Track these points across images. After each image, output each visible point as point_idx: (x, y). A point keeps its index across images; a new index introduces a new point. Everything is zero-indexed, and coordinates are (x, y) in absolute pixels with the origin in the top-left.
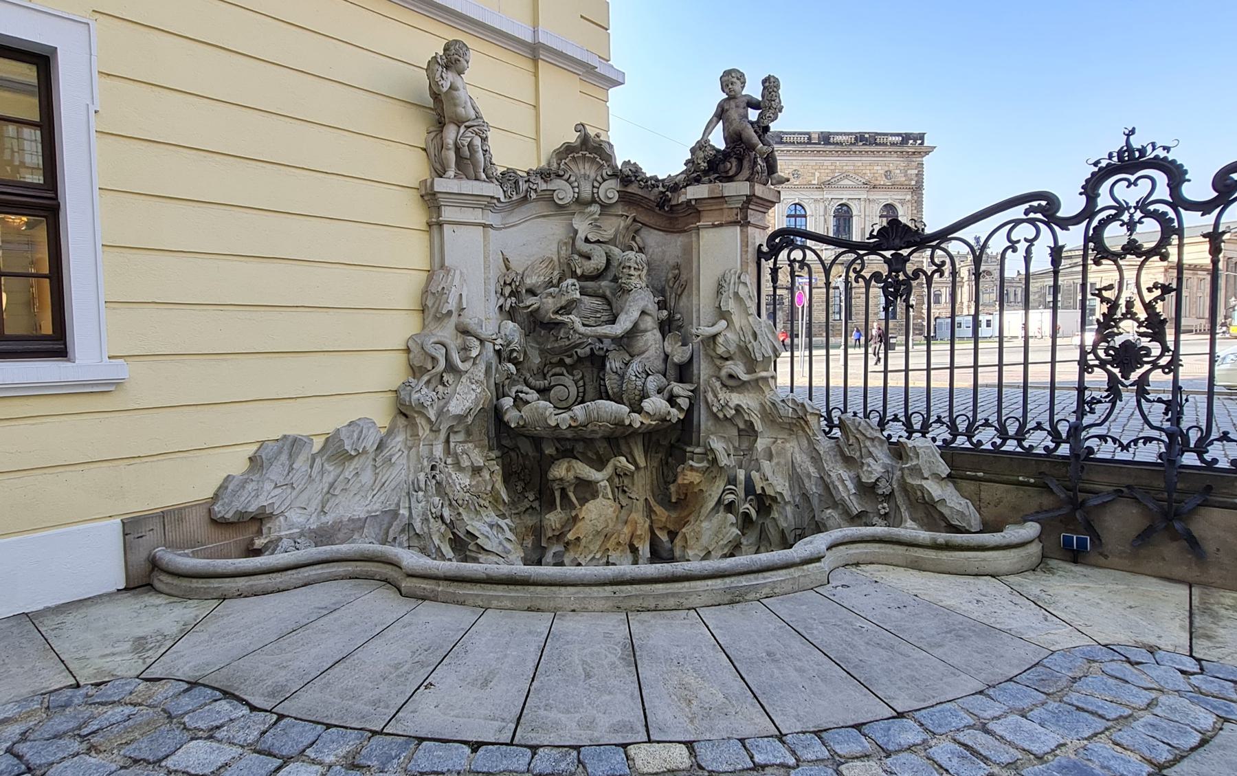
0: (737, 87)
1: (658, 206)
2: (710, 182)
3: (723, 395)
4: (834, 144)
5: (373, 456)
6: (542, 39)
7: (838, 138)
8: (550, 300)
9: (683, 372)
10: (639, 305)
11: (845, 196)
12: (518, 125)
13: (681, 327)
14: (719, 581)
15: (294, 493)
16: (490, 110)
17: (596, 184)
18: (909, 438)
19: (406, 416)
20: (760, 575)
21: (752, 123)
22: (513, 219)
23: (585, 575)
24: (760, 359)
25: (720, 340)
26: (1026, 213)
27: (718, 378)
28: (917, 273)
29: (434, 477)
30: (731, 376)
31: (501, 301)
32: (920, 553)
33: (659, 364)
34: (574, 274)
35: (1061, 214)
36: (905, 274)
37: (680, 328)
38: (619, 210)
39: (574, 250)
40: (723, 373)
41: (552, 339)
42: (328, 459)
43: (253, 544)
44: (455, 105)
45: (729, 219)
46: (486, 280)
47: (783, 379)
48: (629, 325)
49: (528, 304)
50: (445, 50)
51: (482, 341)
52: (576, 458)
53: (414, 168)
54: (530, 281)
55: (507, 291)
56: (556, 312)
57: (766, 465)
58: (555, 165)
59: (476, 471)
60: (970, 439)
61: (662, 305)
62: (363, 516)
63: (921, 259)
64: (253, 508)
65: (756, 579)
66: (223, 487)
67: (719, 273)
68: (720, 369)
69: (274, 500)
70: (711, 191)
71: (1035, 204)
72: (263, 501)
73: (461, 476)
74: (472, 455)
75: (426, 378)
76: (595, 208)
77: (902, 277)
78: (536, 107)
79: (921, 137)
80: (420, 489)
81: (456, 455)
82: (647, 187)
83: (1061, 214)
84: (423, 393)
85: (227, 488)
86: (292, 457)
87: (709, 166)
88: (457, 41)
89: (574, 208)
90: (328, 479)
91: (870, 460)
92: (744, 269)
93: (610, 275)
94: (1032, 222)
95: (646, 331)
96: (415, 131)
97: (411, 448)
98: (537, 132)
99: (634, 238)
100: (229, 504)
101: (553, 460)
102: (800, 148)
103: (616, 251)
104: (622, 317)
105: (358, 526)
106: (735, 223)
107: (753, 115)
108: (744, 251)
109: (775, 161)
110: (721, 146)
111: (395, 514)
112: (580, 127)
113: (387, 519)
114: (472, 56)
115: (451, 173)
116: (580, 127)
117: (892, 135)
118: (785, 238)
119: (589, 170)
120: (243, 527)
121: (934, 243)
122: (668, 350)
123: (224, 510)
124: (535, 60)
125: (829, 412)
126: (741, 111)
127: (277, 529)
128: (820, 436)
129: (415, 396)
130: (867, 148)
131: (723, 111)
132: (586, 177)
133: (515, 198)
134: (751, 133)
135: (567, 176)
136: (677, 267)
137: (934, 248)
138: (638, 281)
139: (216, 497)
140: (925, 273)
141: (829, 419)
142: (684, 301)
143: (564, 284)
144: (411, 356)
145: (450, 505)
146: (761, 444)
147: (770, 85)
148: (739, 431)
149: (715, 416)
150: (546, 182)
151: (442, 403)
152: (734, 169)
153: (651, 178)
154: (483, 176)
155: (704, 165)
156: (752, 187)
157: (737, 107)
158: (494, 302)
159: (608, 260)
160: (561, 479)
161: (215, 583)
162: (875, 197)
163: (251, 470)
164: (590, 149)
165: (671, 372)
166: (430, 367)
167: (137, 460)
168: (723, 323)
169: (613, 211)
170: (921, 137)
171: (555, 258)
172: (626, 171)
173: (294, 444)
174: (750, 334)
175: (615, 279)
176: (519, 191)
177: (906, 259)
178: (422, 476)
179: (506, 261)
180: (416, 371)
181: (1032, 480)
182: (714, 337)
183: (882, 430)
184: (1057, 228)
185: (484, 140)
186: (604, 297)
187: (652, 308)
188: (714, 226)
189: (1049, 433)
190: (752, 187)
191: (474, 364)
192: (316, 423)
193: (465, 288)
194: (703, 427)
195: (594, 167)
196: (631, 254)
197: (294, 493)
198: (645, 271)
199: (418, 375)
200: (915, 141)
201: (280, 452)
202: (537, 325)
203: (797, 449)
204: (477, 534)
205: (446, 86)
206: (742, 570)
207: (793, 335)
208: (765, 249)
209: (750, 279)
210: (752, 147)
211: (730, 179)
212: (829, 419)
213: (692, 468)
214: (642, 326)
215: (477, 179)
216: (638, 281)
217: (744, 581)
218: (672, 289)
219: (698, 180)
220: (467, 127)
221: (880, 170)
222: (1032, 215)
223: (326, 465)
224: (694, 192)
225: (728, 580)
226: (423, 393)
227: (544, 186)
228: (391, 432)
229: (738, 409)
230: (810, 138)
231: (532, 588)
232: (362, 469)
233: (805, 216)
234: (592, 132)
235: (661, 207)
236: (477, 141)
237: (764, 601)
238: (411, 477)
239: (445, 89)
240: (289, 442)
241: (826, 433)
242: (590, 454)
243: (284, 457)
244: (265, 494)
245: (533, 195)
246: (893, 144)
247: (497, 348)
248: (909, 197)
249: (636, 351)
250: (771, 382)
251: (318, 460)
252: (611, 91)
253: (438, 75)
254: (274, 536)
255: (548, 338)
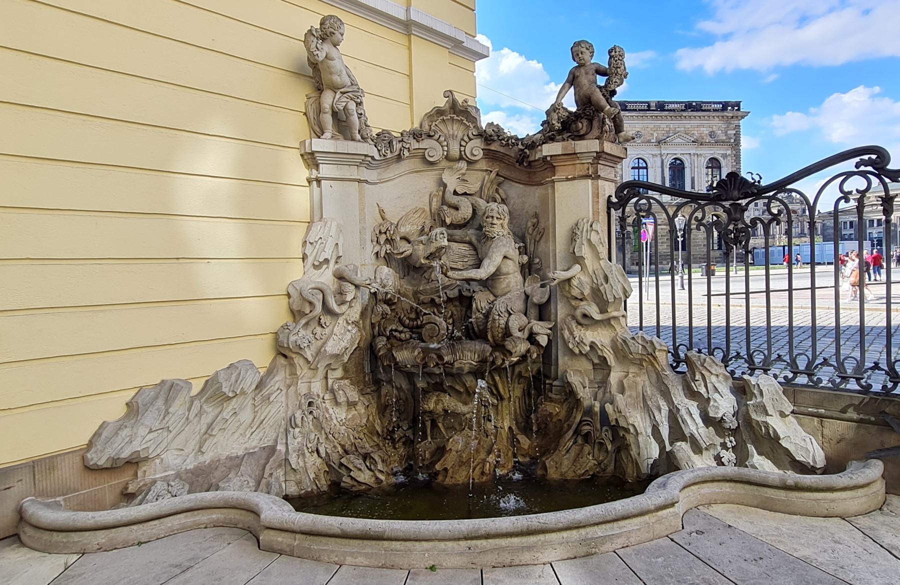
0: (587, 56)
1: (517, 162)
2: (564, 140)
3: (579, 332)
4: (668, 110)
5: (253, 395)
6: (414, 17)
7: (671, 106)
8: (421, 247)
9: (543, 312)
10: (503, 255)
11: (678, 152)
12: (391, 89)
13: (539, 270)
14: (574, 532)
15: (171, 436)
16: (365, 79)
17: (463, 143)
18: (751, 375)
19: (285, 356)
20: (615, 524)
21: (600, 88)
22: (387, 175)
23: (439, 531)
24: (611, 300)
25: (575, 282)
26: (857, 166)
27: (574, 317)
28: (754, 221)
29: (311, 413)
30: (585, 316)
31: (377, 248)
32: (770, 493)
33: (519, 305)
34: (443, 223)
35: (891, 167)
36: (744, 223)
37: (538, 271)
38: (483, 165)
39: (444, 202)
40: (578, 313)
41: (424, 281)
42: (206, 401)
43: (127, 488)
44: (331, 73)
45: (581, 173)
46: (362, 231)
47: (633, 320)
48: (492, 270)
49: (401, 251)
50: (321, 24)
51: (357, 287)
52: (445, 392)
53: (295, 127)
54: (404, 230)
55: (383, 238)
56: (427, 258)
57: (619, 398)
58: (427, 127)
59: (351, 405)
60: (810, 375)
61: (523, 251)
62: (240, 453)
63: (754, 211)
64: (125, 454)
65: (612, 529)
66: (97, 434)
67: (572, 222)
68: (575, 308)
69: (148, 444)
70: (564, 148)
71: (866, 157)
72: (136, 446)
73: (337, 410)
74: (348, 391)
75: (303, 321)
76: (463, 165)
77: (740, 226)
78: (410, 76)
79: (738, 104)
80: (296, 426)
81: (332, 391)
82: (508, 145)
83: (891, 167)
84: (301, 335)
85: (100, 435)
86: (168, 401)
87: (563, 126)
88: (331, 16)
89: (444, 164)
90: (206, 420)
91: (716, 396)
92: (596, 219)
93: (476, 223)
94: (863, 174)
95: (508, 274)
96: (298, 96)
97: (289, 386)
98: (411, 98)
99: (497, 191)
100: (101, 452)
101: (425, 392)
102: (642, 114)
103: (482, 203)
104: (486, 262)
105: (235, 463)
106: (588, 176)
107: (601, 81)
108: (596, 202)
109: (621, 121)
110: (573, 109)
111: (272, 450)
112: (449, 94)
113: (264, 455)
114: (347, 29)
115: (328, 134)
116: (449, 94)
117: (715, 103)
118: (630, 190)
119: (457, 130)
120: (115, 474)
121: (771, 194)
122: (529, 290)
123: (99, 458)
124: (409, 35)
125: (676, 349)
126: (591, 77)
127: (150, 472)
128: (668, 372)
129: (293, 338)
130: (695, 114)
131: (574, 77)
132: (454, 137)
133: (389, 155)
134: (599, 96)
135: (437, 136)
136: (536, 216)
137: (770, 199)
138: (500, 229)
139: (90, 444)
140: (762, 222)
141: (676, 355)
142: (542, 246)
143: (433, 233)
144: (291, 300)
145: (327, 438)
146: (614, 377)
147: (615, 55)
148: (594, 364)
149: (571, 352)
150: (418, 141)
151: (320, 343)
152: (585, 129)
153: (512, 137)
154: (358, 137)
155: (558, 126)
156: (601, 144)
157: (587, 73)
158: (370, 249)
159: (474, 210)
160: (431, 412)
161: (75, 537)
162: (701, 152)
163: (127, 416)
164: (459, 112)
165: (533, 312)
166: (308, 311)
167: (8, 412)
168: (577, 267)
169: (478, 166)
170: (738, 104)
171: (427, 209)
172: (490, 131)
173: (169, 390)
174: (602, 276)
175: (480, 228)
176: (391, 149)
177: (744, 209)
178: (298, 415)
179: (382, 212)
180: (296, 314)
181: (873, 419)
182: (569, 280)
183: (726, 366)
184: (887, 180)
185: (359, 104)
186: (470, 243)
187: (513, 253)
188: (568, 179)
189: (887, 373)
190: (601, 144)
191: (350, 307)
192: (195, 368)
193: (341, 238)
194: (560, 362)
195: (462, 128)
196: (494, 205)
197: (171, 436)
198: (507, 221)
199: (298, 318)
200: (733, 108)
201: (156, 398)
202: (409, 267)
203: (647, 383)
204: (351, 467)
205: (321, 56)
206: (597, 520)
207: (640, 264)
208: (614, 200)
209: (601, 226)
210: (600, 109)
211: (581, 137)
212: (676, 355)
213: (551, 400)
214: (504, 270)
215: (353, 140)
216: (500, 229)
217: (599, 531)
218: (531, 235)
219: (552, 139)
220: (343, 93)
221: (706, 131)
222: (862, 168)
223: (204, 407)
224: (549, 149)
225: (583, 531)
226: (301, 335)
227: (417, 146)
228: (270, 372)
229: (593, 346)
230: (649, 106)
231: (386, 543)
232: (241, 409)
233: (646, 168)
234: (460, 99)
235: (521, 163)
236: (352, 106)
237: (620, 552)
238: (290, 413)
239: (321, 59)
240: (167, 386)
241: (674, 368)
242: (458, 387)
243: (160, 403)
244: (139, 439)
245: (406, 153)
246: (715, 110)
247: (372, 291)
248: (729, 152)
249: (499, 292)
250: (622, 320)
251: (197, 403)
252: (477, 63)
253: (313, 45)
254: (149, 477)
255: (420, 281)
